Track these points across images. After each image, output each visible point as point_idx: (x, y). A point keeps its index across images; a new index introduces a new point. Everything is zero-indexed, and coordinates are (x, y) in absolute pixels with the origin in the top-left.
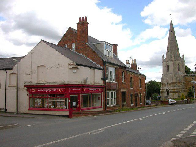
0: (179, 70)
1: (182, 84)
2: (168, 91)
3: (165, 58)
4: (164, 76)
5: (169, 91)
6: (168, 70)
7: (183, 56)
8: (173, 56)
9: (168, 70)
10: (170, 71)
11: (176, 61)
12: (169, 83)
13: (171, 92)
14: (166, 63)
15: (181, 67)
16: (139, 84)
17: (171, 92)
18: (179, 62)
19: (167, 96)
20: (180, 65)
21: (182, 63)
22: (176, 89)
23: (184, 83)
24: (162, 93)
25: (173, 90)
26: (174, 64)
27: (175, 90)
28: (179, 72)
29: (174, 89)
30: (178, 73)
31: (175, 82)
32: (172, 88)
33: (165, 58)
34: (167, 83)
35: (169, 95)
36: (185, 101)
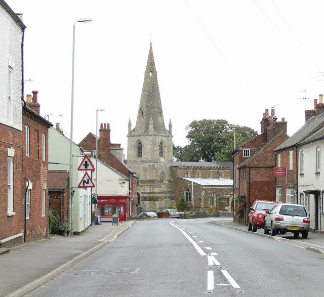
0: (161, 155)
1: (167, 182)
7: (170, 126)
23: (169, 181)
25: (148, 195)
28: (162, 160)
29: (153, 193)
30: (159, 160)
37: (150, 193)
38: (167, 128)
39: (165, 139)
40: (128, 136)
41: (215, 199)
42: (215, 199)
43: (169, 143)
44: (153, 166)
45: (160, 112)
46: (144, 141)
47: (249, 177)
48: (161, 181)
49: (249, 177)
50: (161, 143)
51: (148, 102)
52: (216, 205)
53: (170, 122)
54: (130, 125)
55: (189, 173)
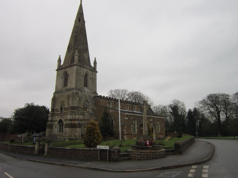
0: (86, 85)
1: (90, 111)
2: (62, 124)
3: (62, 63)
4: (57, 95)
5: (65, 123)
6: (65, 84)
7: (95, 63)
8: (76, 58)
9: (65, 84)
10: (68, 84)
11: (82, 69)
12: (65, 109)
13: (68, 126)
14: (63, 71)
15: (90, 80)
16: (143, 170)
17: (66, 125)
18: (88, 70)
19: (59, 134)
20: (89, 78)
21: (93, 75)
22: (78, 120)
23: (93, 109)
24: (51, 127)
25: (70, 122)
26: (77, 73)
27: (76, 122)
28: (86, 90)
29: (75, 120)
30: (84, 89)
31: (76, 106)
32: (69, 117)
33: (62, 63)
34: (61, 109)
35: (62, 132)
36: (102, 151)
37: (71, 120)
38: (92, 65)
39: (90, 73)
40: (57, 70)
41: (136, 126)
42: (136, 126)
43: (93, 76)
44: (77, 93)
45: (86, 50)
46: (69, 70)
47: (130, 134)
48: (85, 108)
49: (130, 134)
50: (86, 75)
51: (75, 43)
52: (137, 132)
53: (95, 60)
54: (60, 60)
55: (111, 104)
